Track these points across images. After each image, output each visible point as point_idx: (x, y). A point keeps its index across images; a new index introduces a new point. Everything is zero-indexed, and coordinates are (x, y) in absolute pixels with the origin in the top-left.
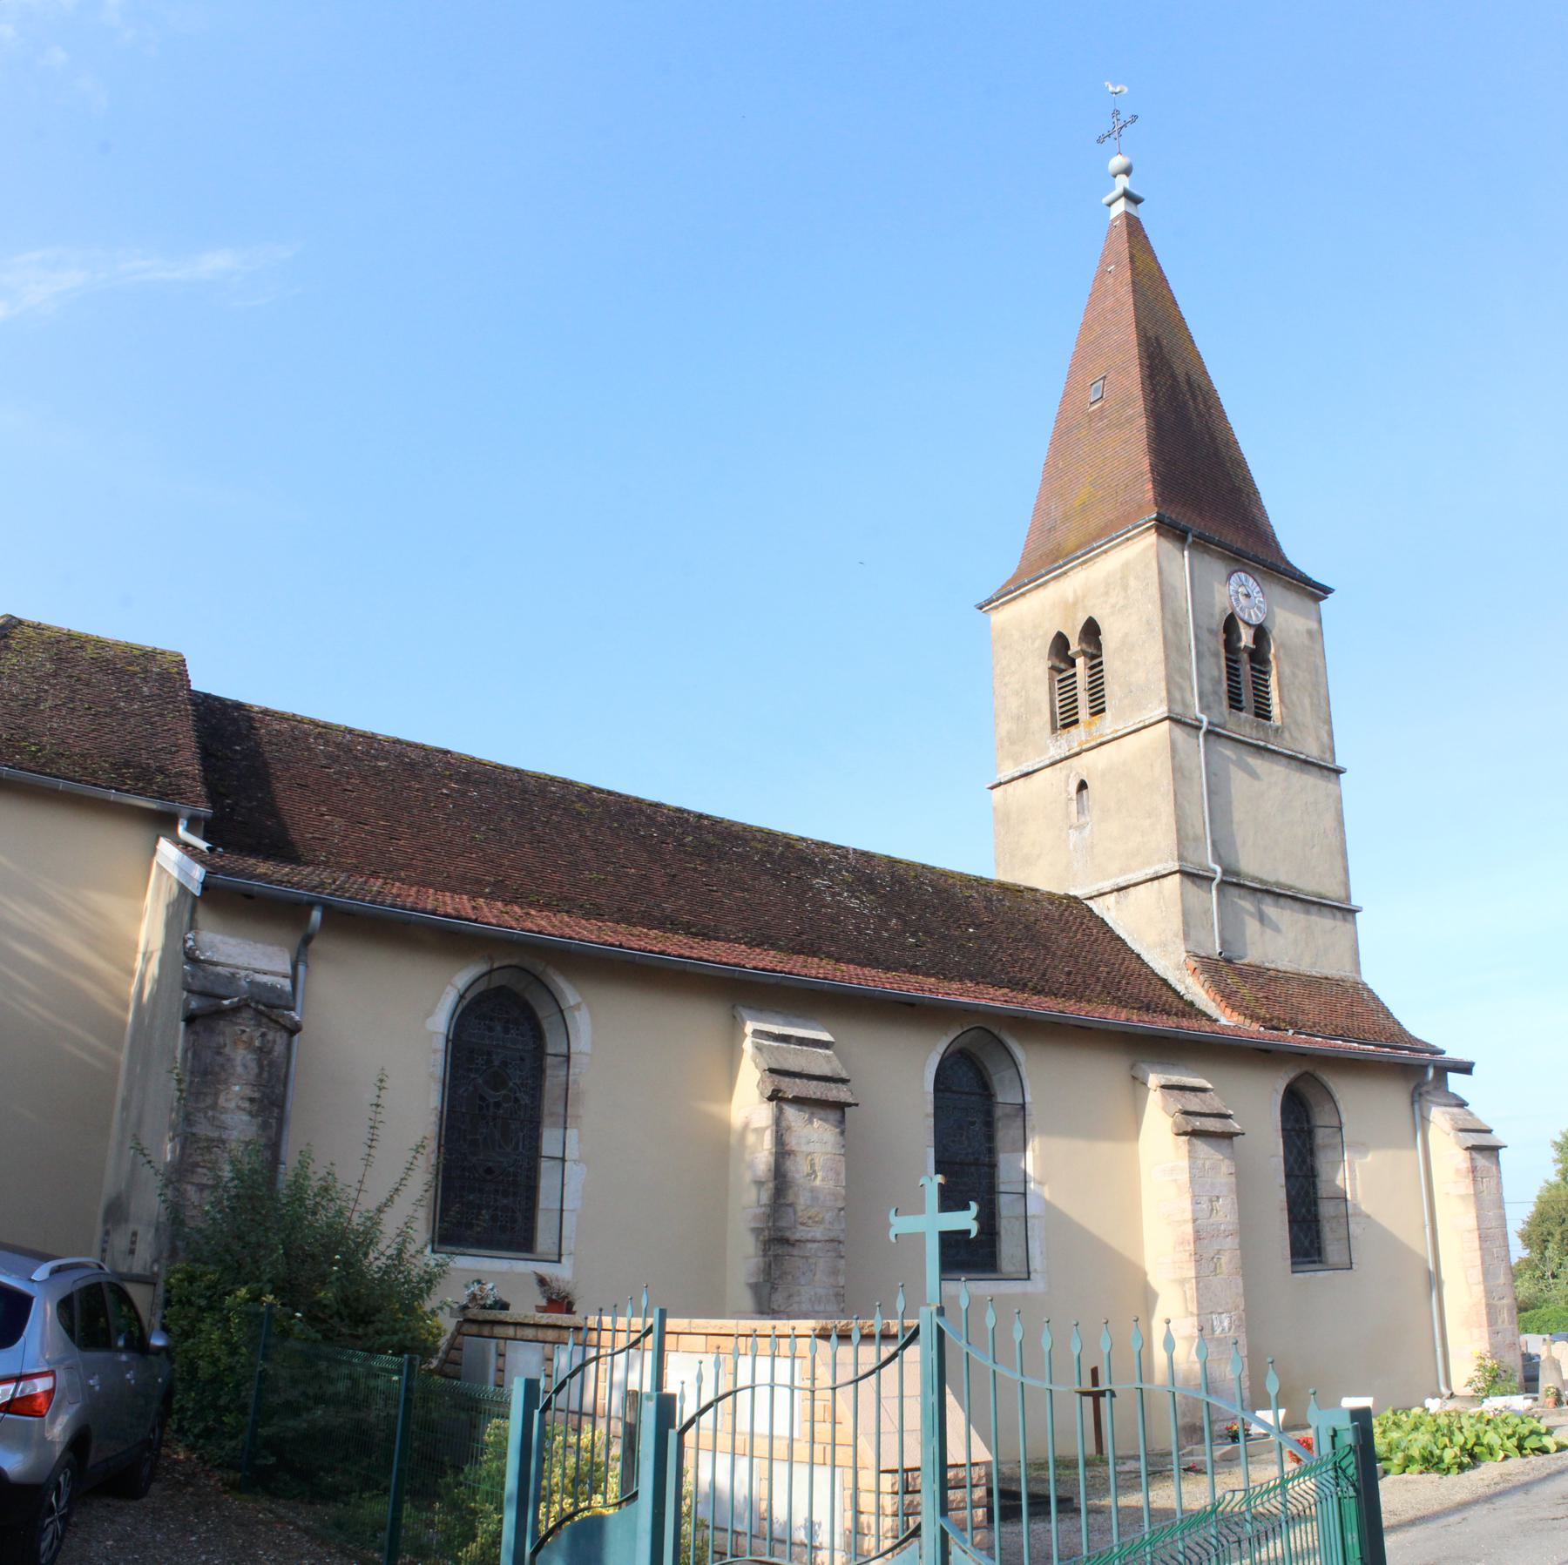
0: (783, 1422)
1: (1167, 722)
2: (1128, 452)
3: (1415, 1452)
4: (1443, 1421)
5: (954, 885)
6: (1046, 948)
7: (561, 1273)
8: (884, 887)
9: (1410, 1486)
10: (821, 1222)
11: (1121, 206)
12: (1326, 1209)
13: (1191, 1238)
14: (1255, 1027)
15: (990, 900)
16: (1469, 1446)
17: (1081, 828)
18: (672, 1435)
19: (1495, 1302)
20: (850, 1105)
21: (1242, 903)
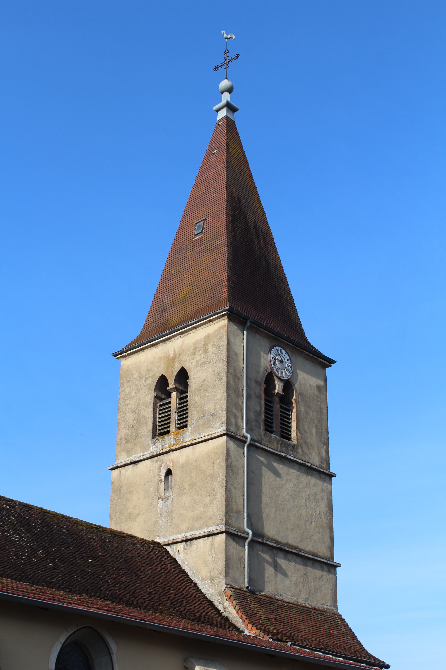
1: (225, 437)
2: (214, 267)
5: (82, 530)
8: (36, 529)
11: (223, 113)
14: (267, 638)
15: (104, 541)
17: (165, 499)
21: (264, 555)
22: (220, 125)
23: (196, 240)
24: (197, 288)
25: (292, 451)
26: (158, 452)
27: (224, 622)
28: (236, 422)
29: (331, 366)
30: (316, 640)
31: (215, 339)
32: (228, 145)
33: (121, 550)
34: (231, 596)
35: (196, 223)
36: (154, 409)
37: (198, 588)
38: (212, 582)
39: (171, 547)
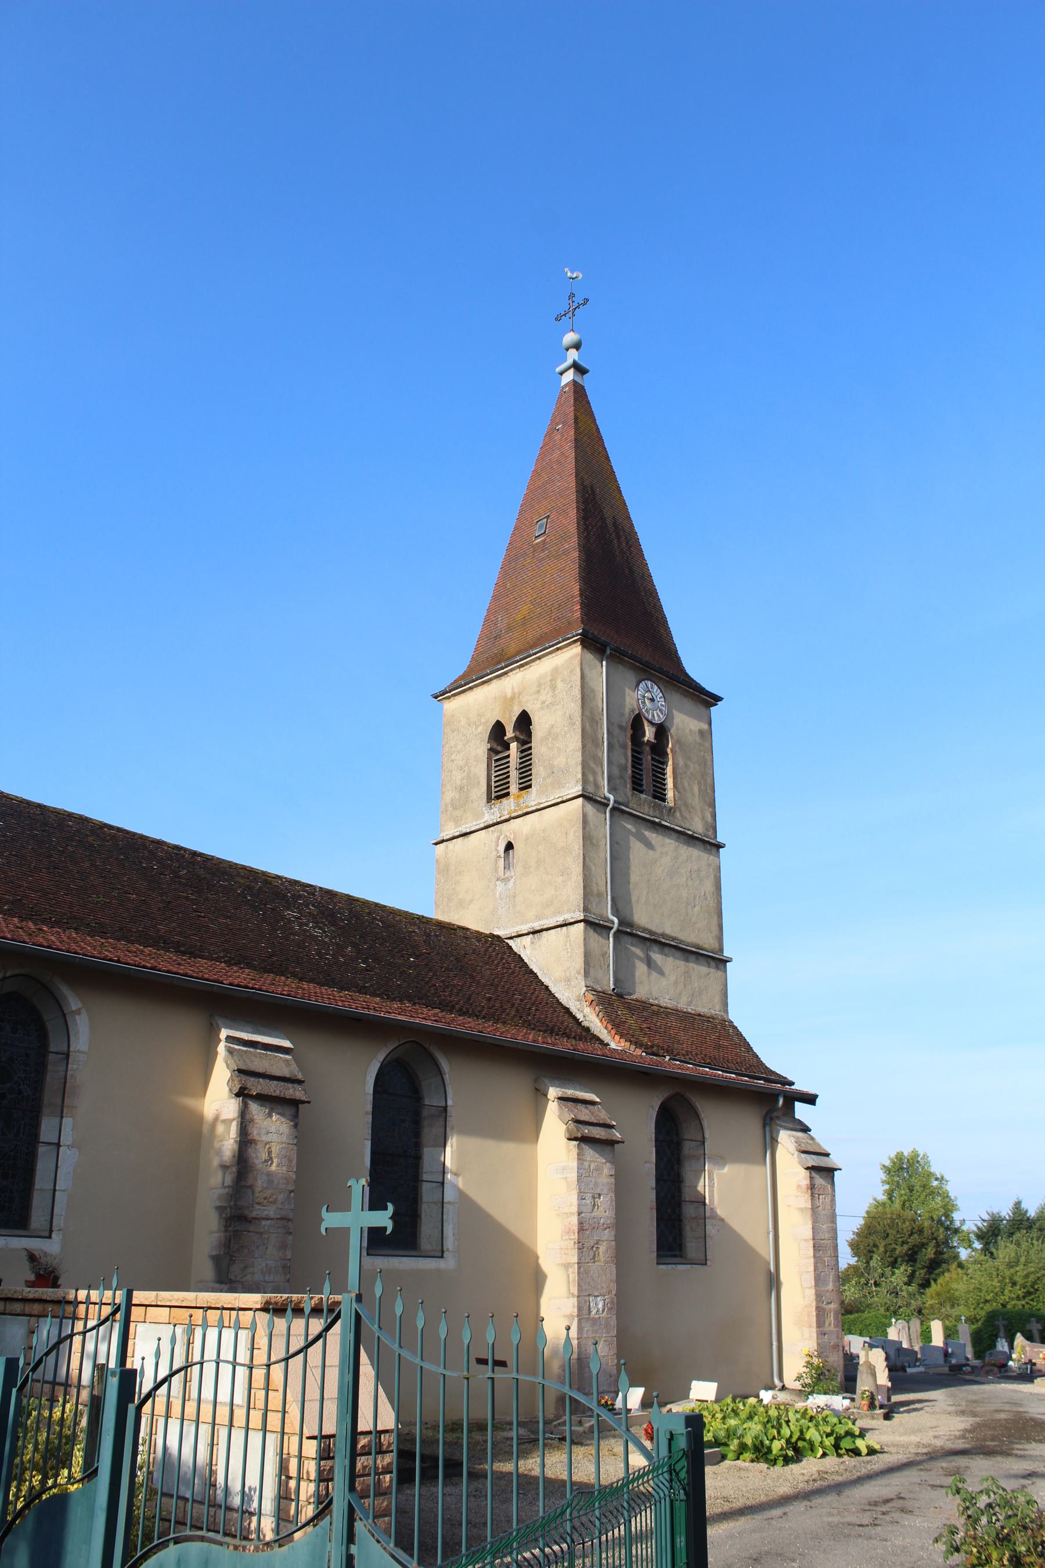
0: (225, 1391)
1: (581, 799)
2: (563, 578)
3: (749, 1441)
4: (773, 1413)
5: (401, 921)
6: (472, 977)
7: (51, 1247)
9: (743, 1474)
10: (274, 1202)
11: (569, 376)
12: (688, 1211)
13: (576, 1228)
14: (638, 1052)
15: (429, 936)
16: (794, 1440)
18: (131, 1408)
19: (824, 1305)
20: (303, 1102)
21: (633, 949)
32: (576, 418)
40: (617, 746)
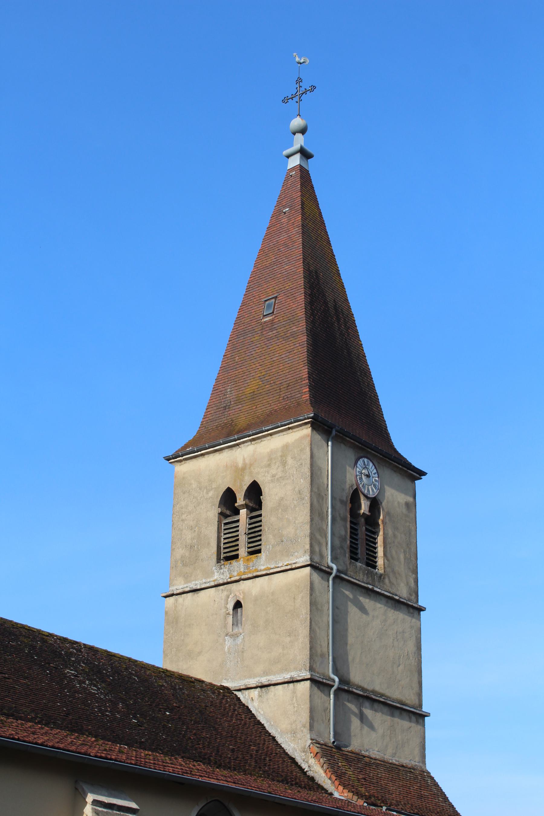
1: (308, 569)
2: (291, 358)
5: (150, 675)
6: (216, 729)
11: (295, 161)
14: (361, 802)
15: (175, 689)
17: (234, 636)
22: (291, 176)
23: (265, 322)
24: (269, 383)
25: (379, 582)
26: (225, 581)
27: (311, 783)
28: (320, 551)
29: (421, 479)
30: (408, 803)
31: (295, 451)
32: (303, 204)
33: (194, 698)
34: (317, 753)
35: (266, 301)
36: (218, 528)
37: (277, 742)
38: (294, 736)
39: (242, 694)
40: (338, 519)
